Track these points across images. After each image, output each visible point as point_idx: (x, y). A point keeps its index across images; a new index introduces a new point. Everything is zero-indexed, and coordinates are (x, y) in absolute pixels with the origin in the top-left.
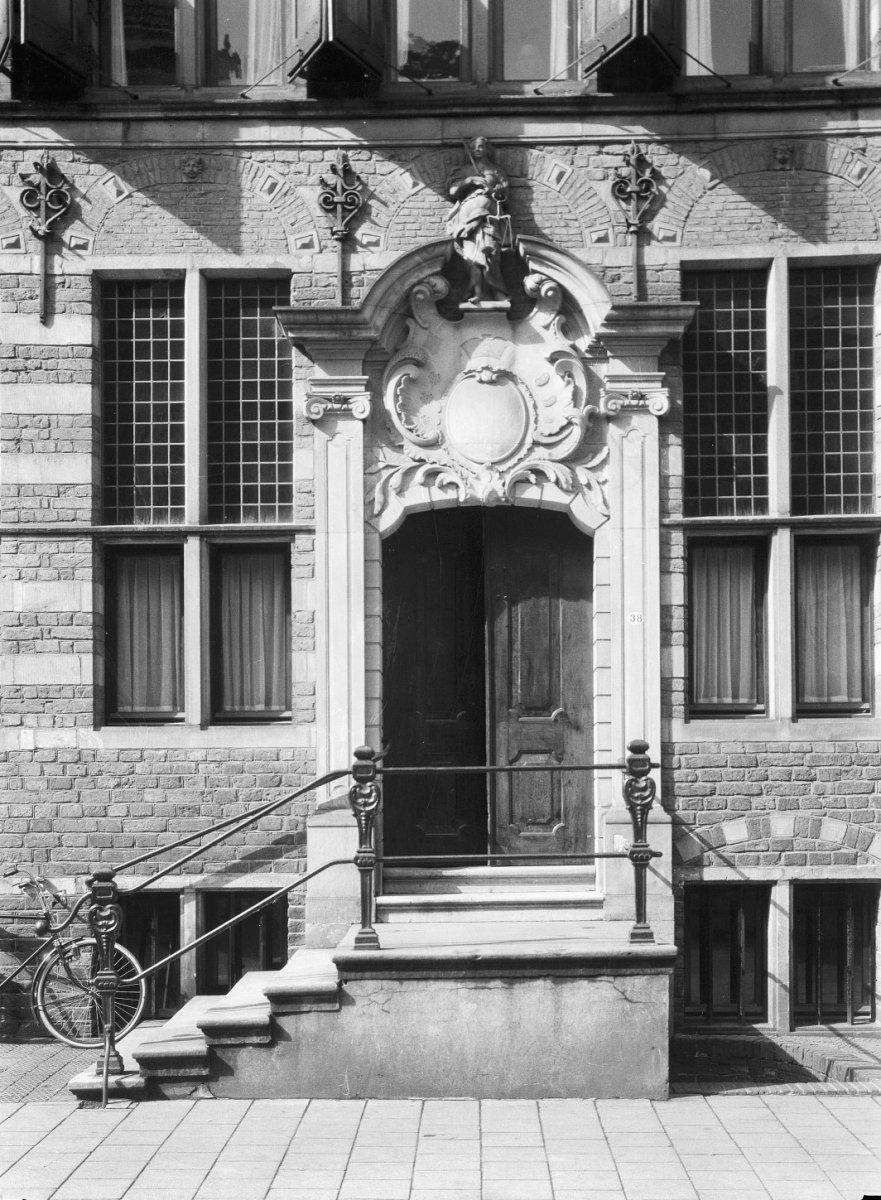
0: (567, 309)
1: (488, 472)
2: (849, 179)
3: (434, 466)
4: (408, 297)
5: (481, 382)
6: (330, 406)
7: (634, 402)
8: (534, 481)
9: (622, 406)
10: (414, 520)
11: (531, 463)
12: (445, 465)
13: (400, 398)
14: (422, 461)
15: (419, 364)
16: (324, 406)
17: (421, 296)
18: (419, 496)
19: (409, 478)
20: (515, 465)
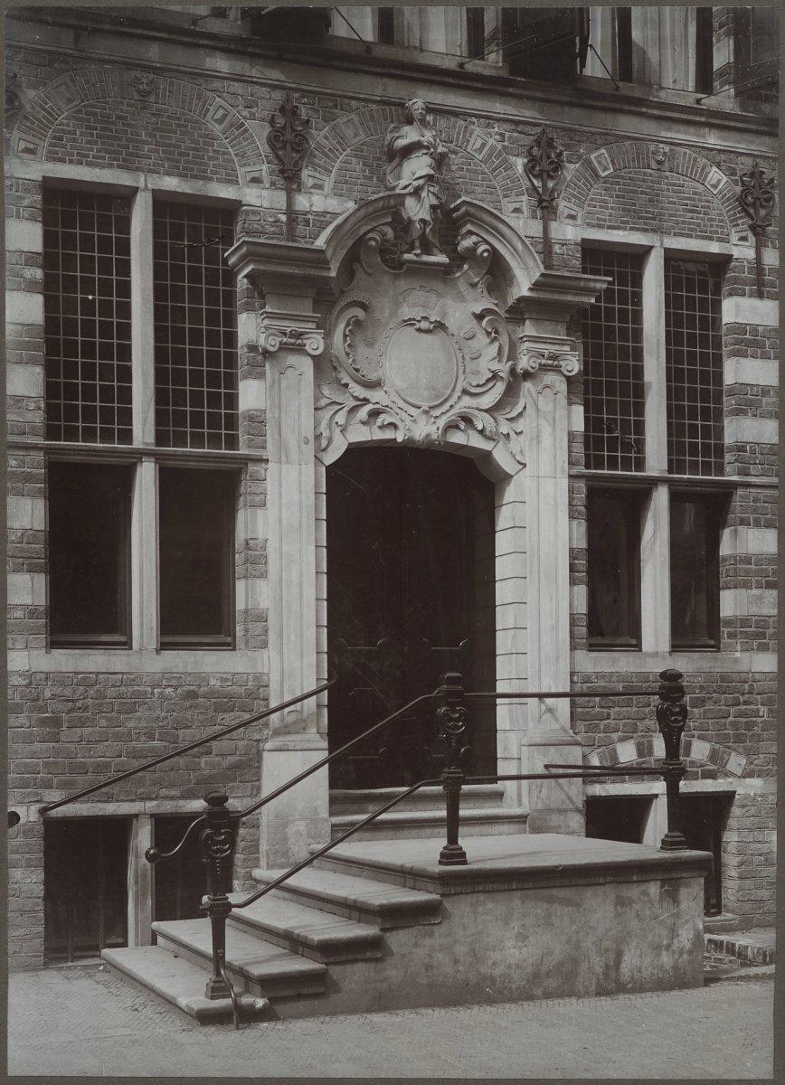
0: (496, 273)
1: (424, 416)
2: (709, 187)
3: (377, 406)
4: (361, 241)
5: (419, 330)
6: (285, 340)
7: (550, 362)
8: (463, 427)
9: (540, 364)
10: (356, 452)
11: (458, 411)
12: (387, 406)
13: (348, 338)
14: (366, 401)
15: (364, 307)
16: (280, 339)
17: (373, 243)
18: (360, 434)
19: (352, 416)
20: (447, 411)
